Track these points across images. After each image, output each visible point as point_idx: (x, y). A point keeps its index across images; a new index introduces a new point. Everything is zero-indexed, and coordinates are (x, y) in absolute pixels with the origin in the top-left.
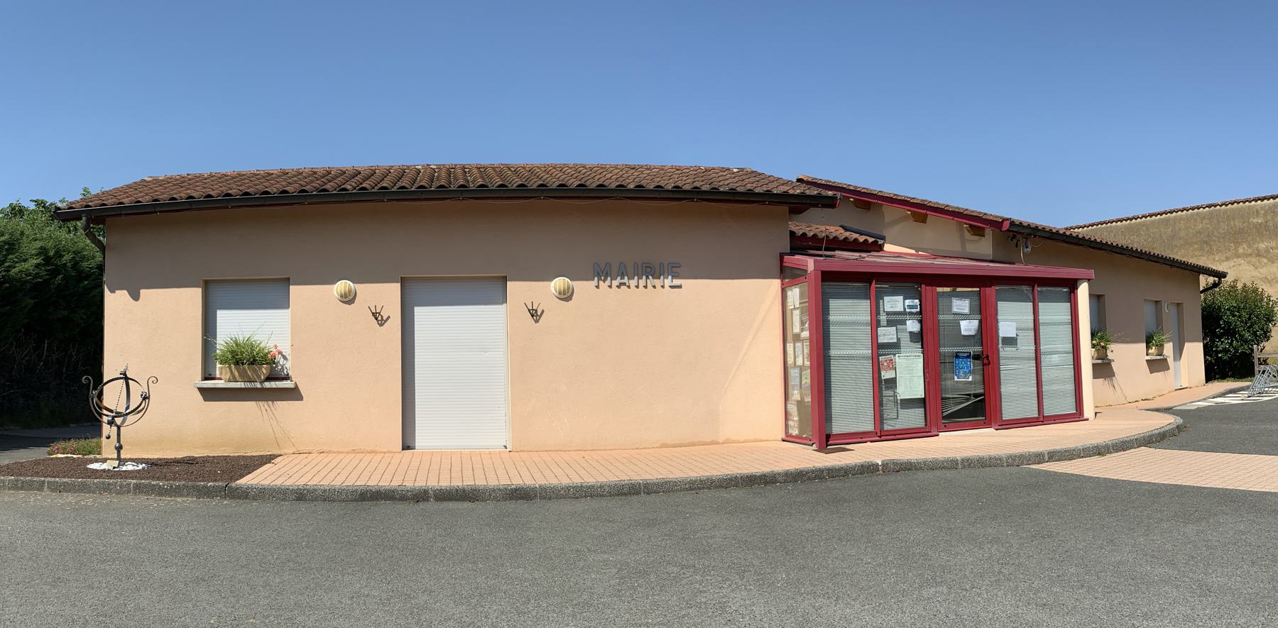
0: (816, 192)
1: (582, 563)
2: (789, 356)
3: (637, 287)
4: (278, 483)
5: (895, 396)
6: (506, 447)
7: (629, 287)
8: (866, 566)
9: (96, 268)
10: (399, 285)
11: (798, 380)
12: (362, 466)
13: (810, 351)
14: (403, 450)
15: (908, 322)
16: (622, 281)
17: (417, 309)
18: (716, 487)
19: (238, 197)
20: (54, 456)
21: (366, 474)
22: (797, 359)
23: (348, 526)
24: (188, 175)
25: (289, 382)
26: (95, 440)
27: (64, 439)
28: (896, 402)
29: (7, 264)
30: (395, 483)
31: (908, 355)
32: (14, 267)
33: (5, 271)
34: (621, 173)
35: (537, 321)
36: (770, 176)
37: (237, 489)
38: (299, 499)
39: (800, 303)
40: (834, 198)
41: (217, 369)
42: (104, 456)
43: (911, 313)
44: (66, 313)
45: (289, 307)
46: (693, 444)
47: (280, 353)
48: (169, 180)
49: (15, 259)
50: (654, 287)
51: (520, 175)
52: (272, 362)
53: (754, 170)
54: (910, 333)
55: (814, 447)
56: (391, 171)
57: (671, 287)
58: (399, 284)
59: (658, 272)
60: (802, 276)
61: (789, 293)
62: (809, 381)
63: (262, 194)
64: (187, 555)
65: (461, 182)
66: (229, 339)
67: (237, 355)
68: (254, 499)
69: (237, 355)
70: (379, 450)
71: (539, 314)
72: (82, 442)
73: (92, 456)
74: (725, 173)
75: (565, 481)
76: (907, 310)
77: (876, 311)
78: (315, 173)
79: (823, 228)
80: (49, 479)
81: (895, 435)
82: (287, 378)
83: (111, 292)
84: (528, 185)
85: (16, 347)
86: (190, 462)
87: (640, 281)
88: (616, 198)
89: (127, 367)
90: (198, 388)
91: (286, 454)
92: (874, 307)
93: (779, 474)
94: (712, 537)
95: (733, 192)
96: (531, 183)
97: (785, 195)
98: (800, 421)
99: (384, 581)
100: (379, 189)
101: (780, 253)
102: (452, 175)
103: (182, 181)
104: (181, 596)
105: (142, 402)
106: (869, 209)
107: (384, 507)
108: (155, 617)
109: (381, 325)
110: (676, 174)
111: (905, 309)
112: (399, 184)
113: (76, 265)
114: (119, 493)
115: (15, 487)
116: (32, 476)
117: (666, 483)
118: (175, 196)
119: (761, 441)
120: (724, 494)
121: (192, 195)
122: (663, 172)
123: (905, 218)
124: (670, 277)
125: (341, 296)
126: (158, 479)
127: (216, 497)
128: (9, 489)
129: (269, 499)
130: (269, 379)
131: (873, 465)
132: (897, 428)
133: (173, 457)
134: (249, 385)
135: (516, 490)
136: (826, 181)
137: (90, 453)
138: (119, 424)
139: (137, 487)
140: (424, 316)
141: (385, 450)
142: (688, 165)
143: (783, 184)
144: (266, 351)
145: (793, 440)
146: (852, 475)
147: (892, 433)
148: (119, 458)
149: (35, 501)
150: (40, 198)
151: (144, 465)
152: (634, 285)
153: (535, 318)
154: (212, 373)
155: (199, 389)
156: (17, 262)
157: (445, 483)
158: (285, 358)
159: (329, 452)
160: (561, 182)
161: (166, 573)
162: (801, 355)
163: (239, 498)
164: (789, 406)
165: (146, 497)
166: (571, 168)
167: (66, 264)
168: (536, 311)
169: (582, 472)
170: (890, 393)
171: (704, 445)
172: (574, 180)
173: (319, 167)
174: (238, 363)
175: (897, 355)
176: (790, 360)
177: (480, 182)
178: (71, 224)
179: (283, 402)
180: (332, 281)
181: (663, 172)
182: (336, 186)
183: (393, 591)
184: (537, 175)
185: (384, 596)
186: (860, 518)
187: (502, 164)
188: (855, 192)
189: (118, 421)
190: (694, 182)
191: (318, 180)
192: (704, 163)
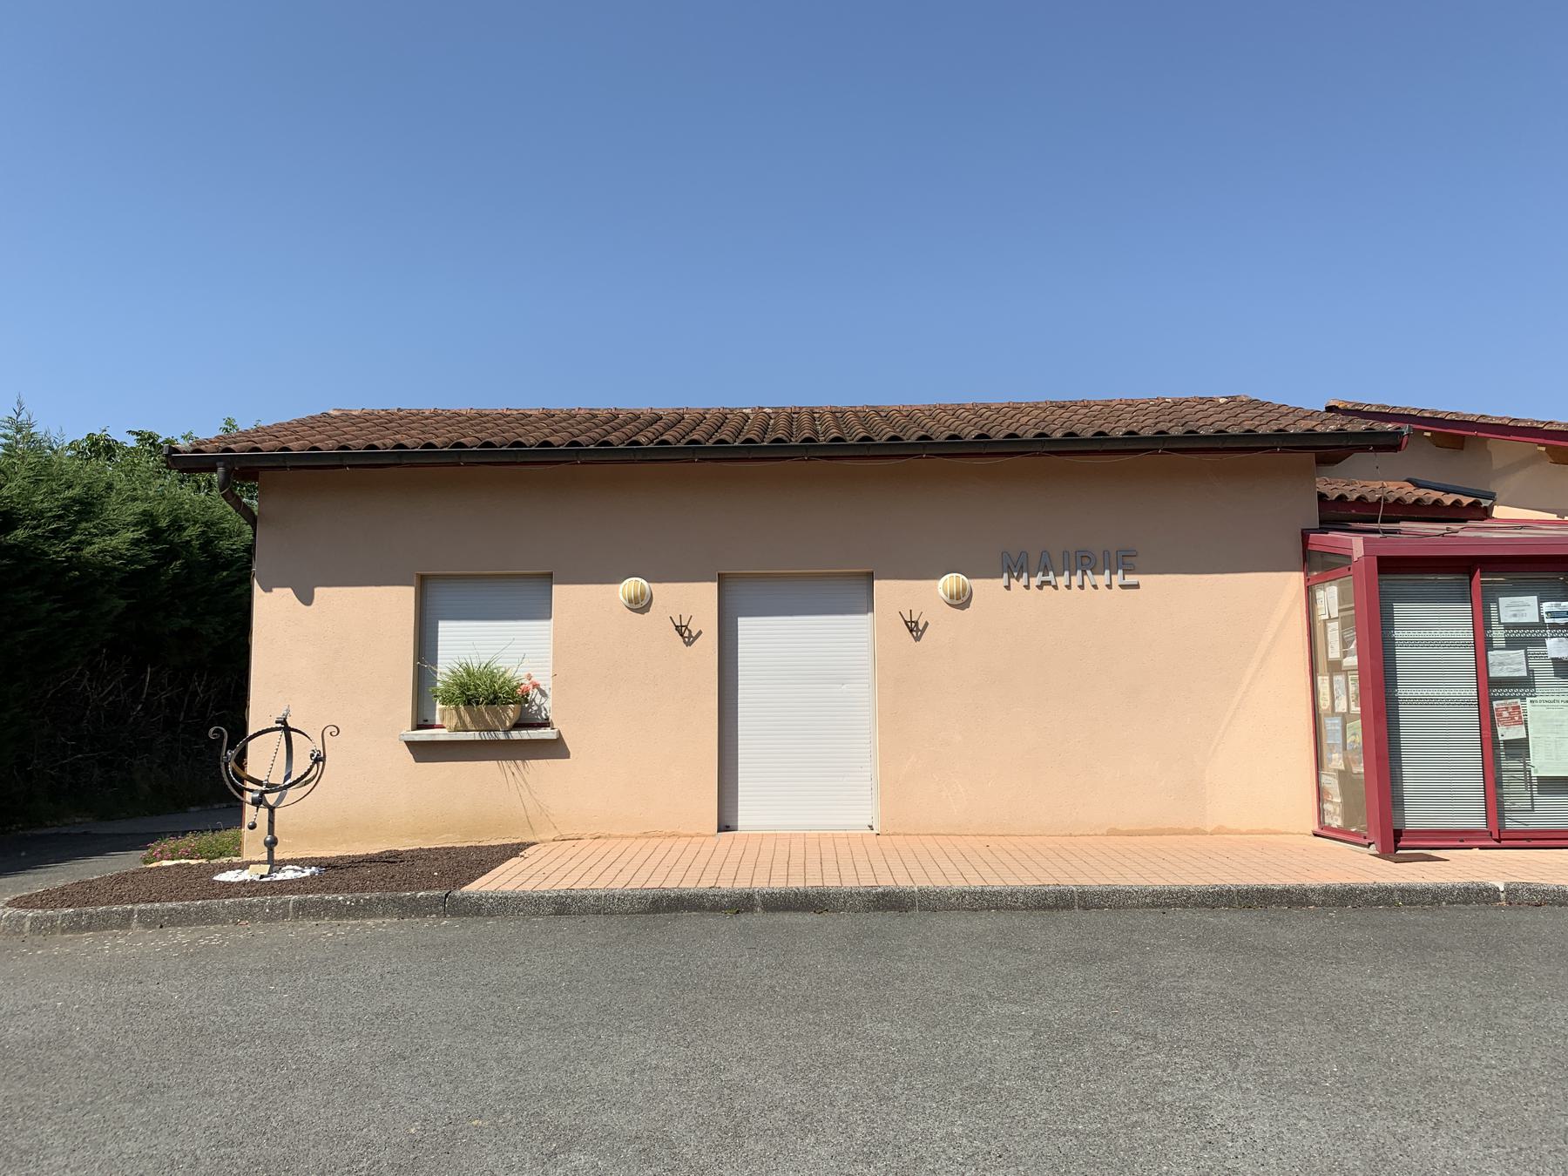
0: (1363, 427)
1: (978, 1018)
2: (1321, 696)
3: (1069, 587)
4: (528, 887)
5: (1526, 771)
7: (1056, 587)
8: (1487, 1071)
9: (244, 551)
11: (1339, 735)
12: (657, 857)
13: (1361, 688)
14: (718, 831)
15: (1548, 642)
16: (1046, 578)
17: (442, 624)
19: (475, 449)
20: (154, 865)
22: (1336, 702)
23: (632, 954)
24: (399, 409)
25: (549, 729)
26: (232, 832)
27: (175, 834)
28: (1528, 781)
29: (76, 538)
30: (705, 884)
31: (1552, 698)
32: (91, 544)
33: (72, 549)
34: (1043, 415)
35: (917, 639)
36: (1280, 407)
37: (463, 899)
38: (558, 913)
39: (1339, 611)
40: (1397, 434)
41: (437, 712)
42: (246, 857)
43: (1554, 626)
44: (187, 622)
45: (550, 617)
46: (1140, 833)
47: (536, 686)
48: (368, 417)
49: (92, 530)
50: (1095, 587)
51: (894, 423)
52: (524, 699)
53: (1254, 398)
54: (1555, 660)
56: (707, 416)
57: (1123, 587)
58: (716, 584)
59: (1100, 564)
61: (1320, 594)
62: (1359, 739)
63: (511, 446)
64: (377, 1015)
65: (807, 434)
66: (457, 666)
67: (469, 690)
68: (490, 914)
69: (469, 690)
70: (685, 832)
71: (921, 627)
72: (208, 837)
73: (224, 860)
74: (1206, 407)
75: (958, 884)
76: (1547, 621)
77: (1482, 624)
78: (595, 416)
79: (1377, 485)
80: (142, 906)
81: (1528, 840)
82: (546, 724)
83: (265, 591)
84: (905, 438)
85: (89, 680)
86: (391, 860)
87: (1072, 578)
88: (1034, 454)
89: (288, 711)
90: (405, 742)
91: (542, 842)
92: (1479, 617)
93: (1312, 890)
94: (1185, 989)
95: (1221, 435)
97: (1310, 434)
98: (1346, 804)
99: (682, 1042)
100: (687, 443)
101: (1303, 530)
103: (388, 420)
104: (364, 1089)
105: (312, 767)
106: (1462, 449)
107: (688, 922)
108: (317, 1134)
109: (688, 644)
110: (1128, 412)
111: (1541, 618)
112: (717, 436)
113: (207, 543)
114: (269, 919)
115: (75, 926)
116: (109, 903)
118: (375, 443)
119: (1276, 833)
120: (1209, 917)
121: (402, 442)
122: (1107, 410)
123: (1536, 458)
124: (1120, 572)
126: (336, 890)
127: (431, 914)
128: (64, 931)
129: (513, 914)
130: (518, 726)
131: (1487, 889)
132: (1532, 826)
133: (363, 853)
134: (486, 736)
135: (884, 895)
136: (1378, 407)
137: (221, 854)
138: (271, 803)
139: (301, 907)
140: (750, 629)
141: (692, 833)
142: (1146, 397)
143: (1303, 418)
144: (515, 684)
145: (1334, 835)
146: (1449, 903)
147: (1522, 836)
148: (271, 860)
149: (113, 948)
150: (147, 429)
151: (313, 868)
152: (1063, 585)
154: (429, 719)
155: (408, 743)
156: (96, 535)
157: (778, 884)
158: (543, 694)
159: (609, 837)
160: (952, 432)
161: (342, 1050)
162: (1343, 696)
163: (466, 914)
164: (1324, 779)
165: (315, 923)
166: (967, 410)
167: (188, 542)
168: (917, 623)
170: (1516, 764)
174: (470, 702)
175: (1528, 699)
176: (1324, 703)
177: (834, 433)
178: (202, 478)
179: (540, 761)
180: (617, 579)
181: (1107, 410)
183: (694, 1059)
185: (681, 1068)
186: (1468, 982)
187: (867, 406)
188: (1434, 421)
189: (271, 798)
191: (597, 426)
192: (1171, 393)
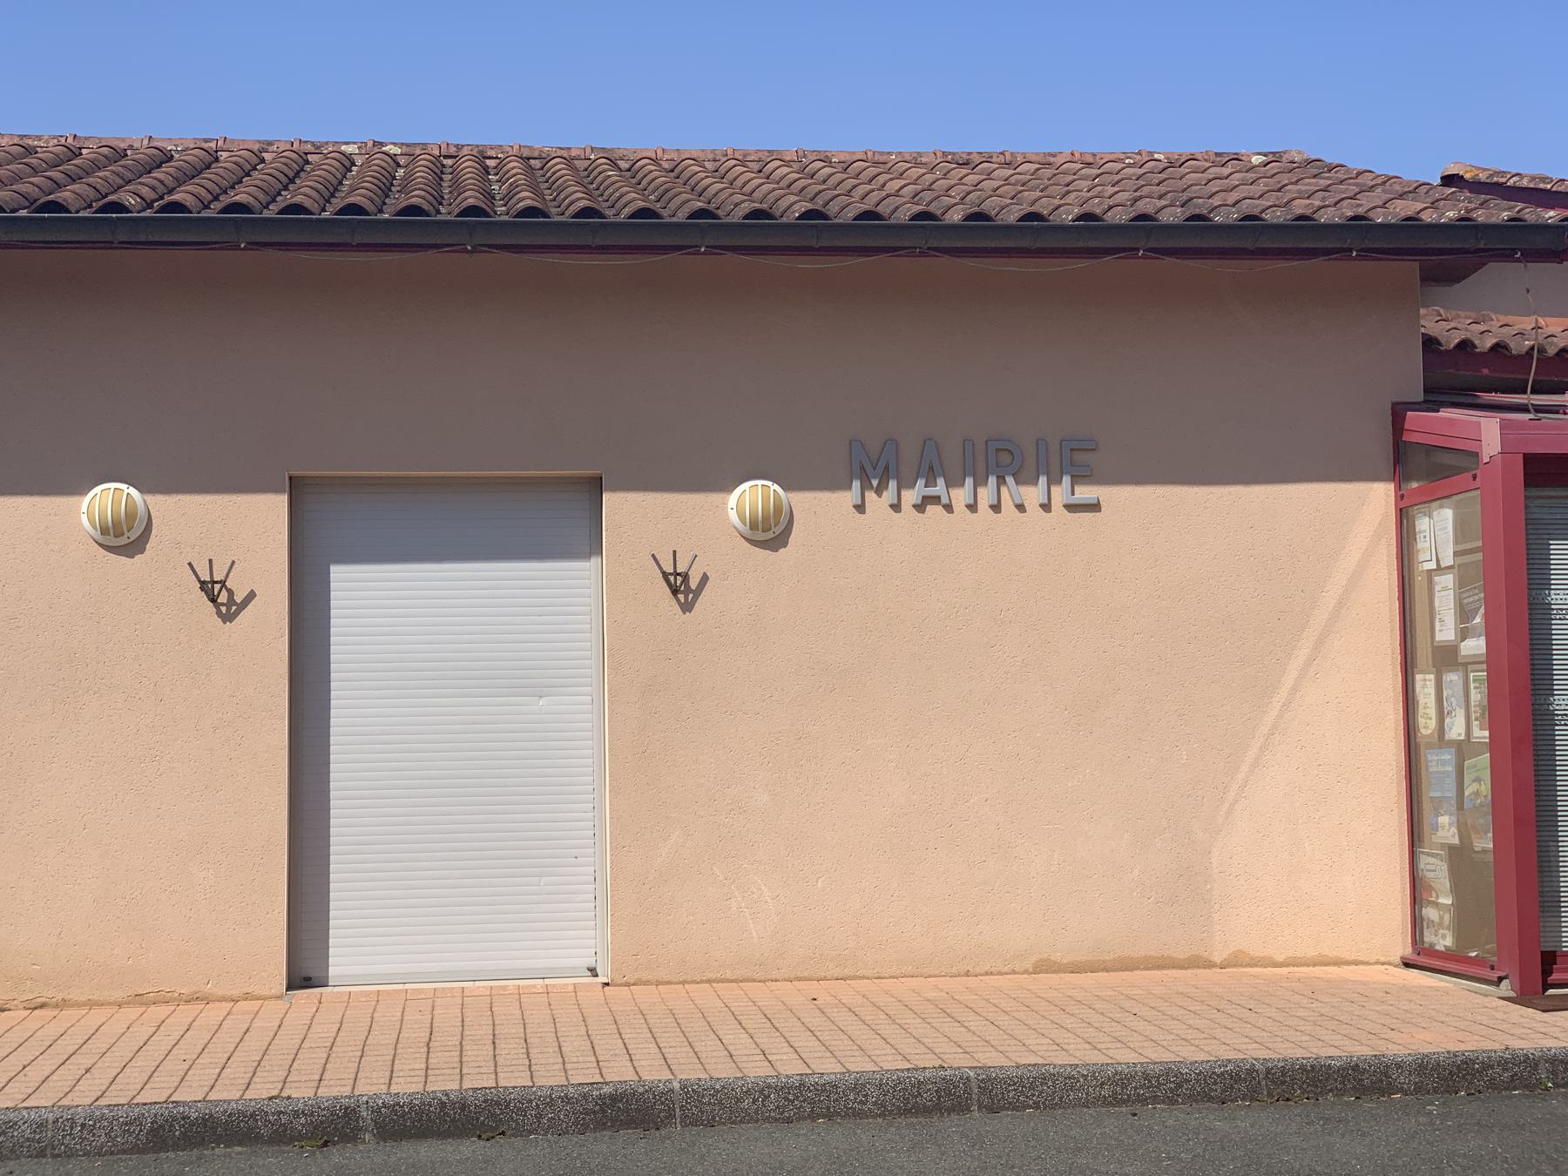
0: (1505, 215)
6: (593, 972)
7: (949, 508)
10: (284, 499)
16: (931, 491)
18: (1192, 1098)
21: (174, 1066)
30: (262, 1090)
34: (929, 178)
35: (687, 607)
36: (1359, 173)
39: (1456, 554)
50: (1021, 508)
51: (644, 182)
55: (1506, 988)
58: (285, 498)
60: (1466, 470)
61: (1423, 524)
62: (1485, 788)
65: (471, 198)
74: (1226, 171)
78: (30, 151)
79: (1527, 323)
88: (910, 252)
93: (1399, 1066)
96: (673, 205)
101: (1394, 405)
102: (447, 177)
109: (228, 618)
112: (287, 198)
117: (1044, 1079)
120: (1214, 1120)
122: (1047, 172)
124: (1066, 480)
125: (104, 531)
135: (614, 1098)
136: (1533, 178)
141: (235, 993)
143: (1401, 196)
152: (962, 505)
153: (681, 597)
159: (63, 1004)
160: (757, 205)
164: (1424, 862)
166: (787, 163)
168: (686, 577)
169: (805, 1043)
171: (1159, 967)
172: (793, 198)
173: (46, 133)
176: (1427, 724)
177: (526, 199)
181: (1047, 172)
182: (92, 193)
184: (692, 182)
190: (1136, 200)
